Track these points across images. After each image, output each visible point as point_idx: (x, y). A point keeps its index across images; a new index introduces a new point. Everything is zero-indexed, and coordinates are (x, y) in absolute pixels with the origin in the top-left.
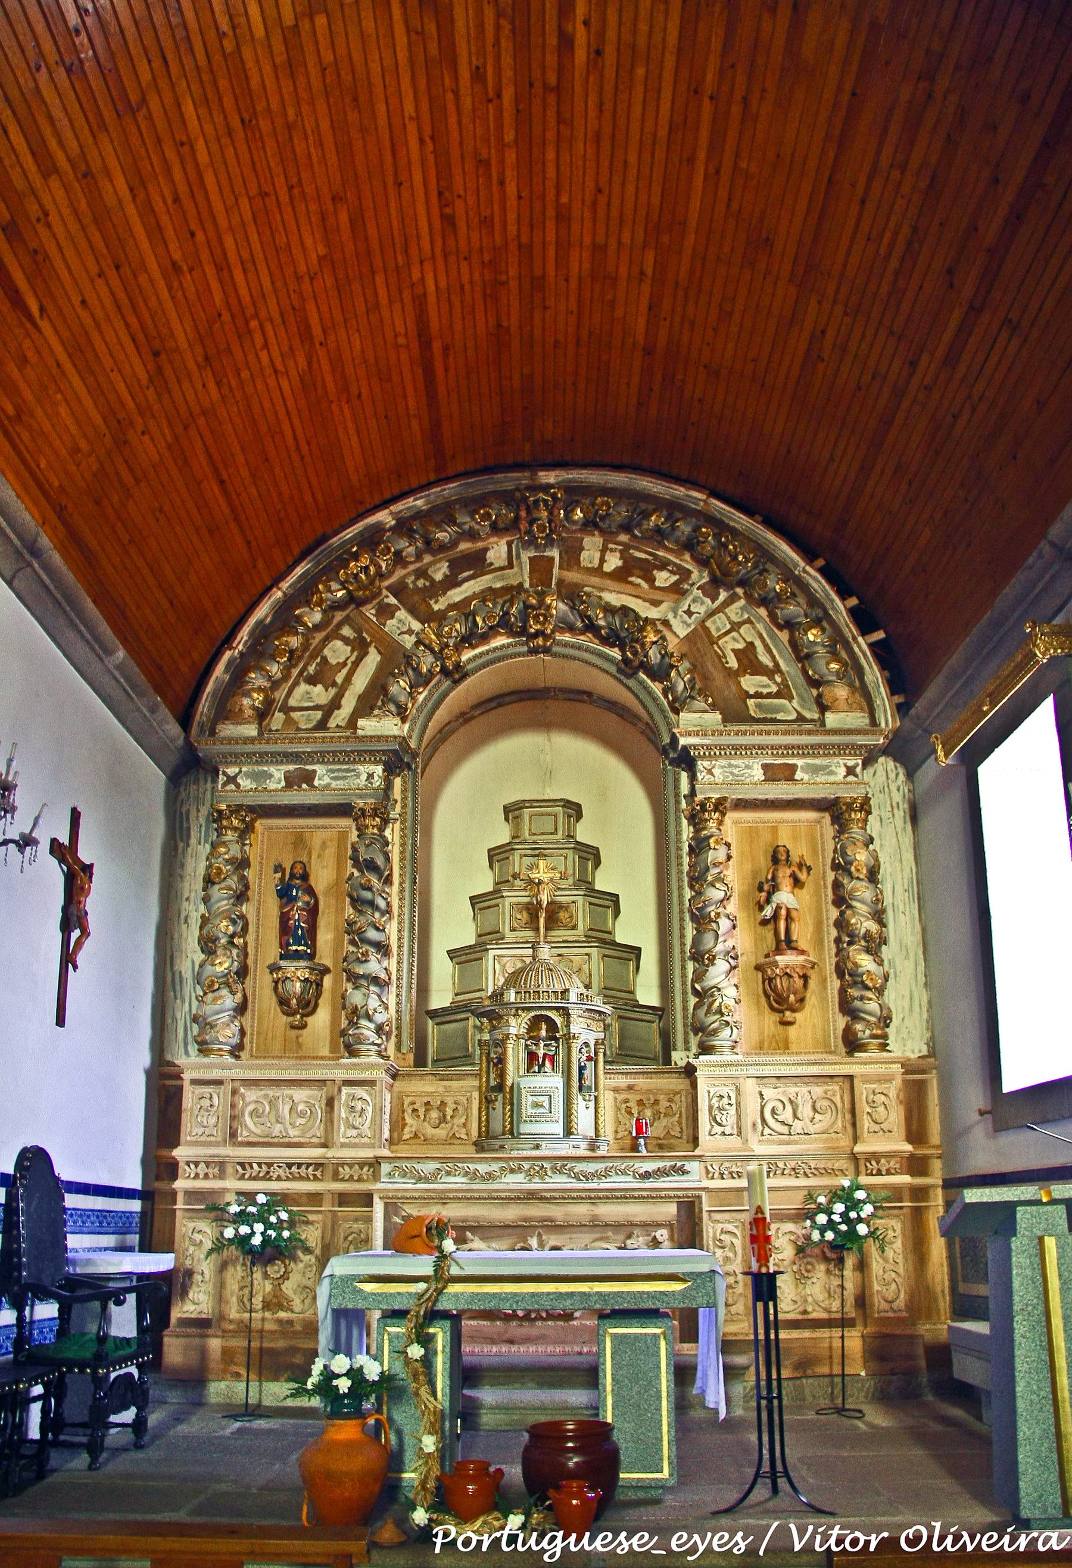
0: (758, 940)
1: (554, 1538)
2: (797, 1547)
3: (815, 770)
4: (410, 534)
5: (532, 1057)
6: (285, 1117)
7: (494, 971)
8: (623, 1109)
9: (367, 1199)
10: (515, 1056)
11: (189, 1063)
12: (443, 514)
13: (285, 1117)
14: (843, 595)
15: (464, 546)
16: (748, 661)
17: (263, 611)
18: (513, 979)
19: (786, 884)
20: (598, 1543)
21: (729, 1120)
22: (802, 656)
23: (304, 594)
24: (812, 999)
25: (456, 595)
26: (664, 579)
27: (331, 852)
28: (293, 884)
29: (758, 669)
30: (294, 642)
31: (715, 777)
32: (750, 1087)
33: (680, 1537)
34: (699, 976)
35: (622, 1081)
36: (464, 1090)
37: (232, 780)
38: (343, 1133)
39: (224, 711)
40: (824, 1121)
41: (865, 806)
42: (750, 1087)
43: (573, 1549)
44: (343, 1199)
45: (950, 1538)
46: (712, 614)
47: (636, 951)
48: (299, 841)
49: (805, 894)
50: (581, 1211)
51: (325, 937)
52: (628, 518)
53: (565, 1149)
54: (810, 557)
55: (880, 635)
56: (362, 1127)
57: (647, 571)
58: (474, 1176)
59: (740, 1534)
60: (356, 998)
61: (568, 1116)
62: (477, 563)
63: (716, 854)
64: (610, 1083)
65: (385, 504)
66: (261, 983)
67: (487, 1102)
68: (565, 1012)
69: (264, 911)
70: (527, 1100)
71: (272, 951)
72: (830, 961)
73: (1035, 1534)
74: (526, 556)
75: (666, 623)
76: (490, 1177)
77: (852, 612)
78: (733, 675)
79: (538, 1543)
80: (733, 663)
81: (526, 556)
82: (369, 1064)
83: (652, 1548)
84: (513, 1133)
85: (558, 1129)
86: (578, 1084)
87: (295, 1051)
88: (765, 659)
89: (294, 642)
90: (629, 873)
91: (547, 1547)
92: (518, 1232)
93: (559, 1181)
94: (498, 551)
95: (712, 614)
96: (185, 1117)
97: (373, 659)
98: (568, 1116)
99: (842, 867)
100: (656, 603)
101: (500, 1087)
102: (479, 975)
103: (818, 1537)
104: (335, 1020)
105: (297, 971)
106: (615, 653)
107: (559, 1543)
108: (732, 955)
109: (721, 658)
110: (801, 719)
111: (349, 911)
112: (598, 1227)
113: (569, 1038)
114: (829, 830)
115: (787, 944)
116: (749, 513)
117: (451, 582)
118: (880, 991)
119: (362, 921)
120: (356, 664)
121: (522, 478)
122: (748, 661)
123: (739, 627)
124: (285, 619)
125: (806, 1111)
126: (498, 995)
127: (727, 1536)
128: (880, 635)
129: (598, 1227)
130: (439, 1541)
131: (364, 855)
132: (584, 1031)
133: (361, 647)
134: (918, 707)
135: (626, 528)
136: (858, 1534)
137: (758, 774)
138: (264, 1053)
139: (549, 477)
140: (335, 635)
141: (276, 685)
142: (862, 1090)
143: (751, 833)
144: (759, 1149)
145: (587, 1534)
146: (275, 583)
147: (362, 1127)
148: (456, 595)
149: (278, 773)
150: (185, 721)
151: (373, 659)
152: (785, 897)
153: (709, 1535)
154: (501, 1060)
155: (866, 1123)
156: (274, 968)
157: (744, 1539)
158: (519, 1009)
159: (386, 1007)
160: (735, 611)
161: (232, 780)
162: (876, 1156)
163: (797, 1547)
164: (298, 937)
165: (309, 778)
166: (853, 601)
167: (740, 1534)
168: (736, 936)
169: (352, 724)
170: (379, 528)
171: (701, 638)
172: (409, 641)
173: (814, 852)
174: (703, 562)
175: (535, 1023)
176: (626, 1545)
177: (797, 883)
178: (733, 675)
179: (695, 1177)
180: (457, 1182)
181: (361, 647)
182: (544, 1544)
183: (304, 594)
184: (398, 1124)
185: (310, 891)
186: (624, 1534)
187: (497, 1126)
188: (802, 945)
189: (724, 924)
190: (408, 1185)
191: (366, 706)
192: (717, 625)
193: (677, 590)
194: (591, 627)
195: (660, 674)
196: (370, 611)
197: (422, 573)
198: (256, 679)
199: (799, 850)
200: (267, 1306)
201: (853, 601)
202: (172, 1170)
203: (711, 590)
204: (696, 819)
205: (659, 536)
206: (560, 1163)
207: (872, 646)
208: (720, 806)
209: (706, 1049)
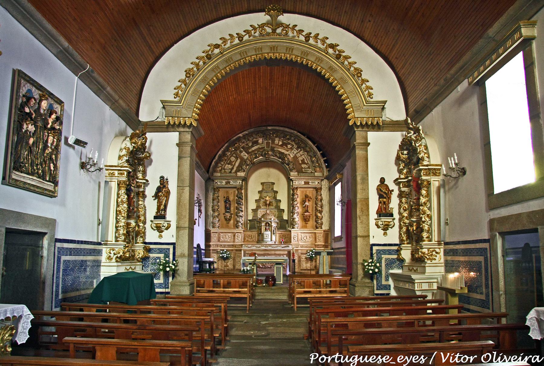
0: (303, 210)
1: (354, 358)
2: (444, 361)
3: (312, 182)
4: (245, 138)
5: (266, 229)
6: (227, 238)
7: (260, 213)
8: (280, 237)
9: (241, 250)
10: (263, 228)
11: (212, 230)
12: (250, 135)
13: (227, 238)
14: (319, 151)
15: (255, 140)
16: (303, 161)
17: (220, 152)
18: (263, 216)
19: (307, 201)
20: (370, 360)
21: (296, 239)
22: (313, 162)
23: (227, 149)
24: (311, 220)
25: (253, 149)
26: (289, 146)
27: (232, 194)
28: (227, 201)
29: (305, 163)
30: (226, 158)
31: (296, 183)
32: (300, 234)
33: (401, 357)
34: (292, 216)
35: (280, 232)
36: (254, 233)
37: (216, 183)
38: (236, 240)
39: (215, 171)
40: (311, 239)
41: (321, 189)
42: (300, 234)
43: (361, 362)
44: (237, 250)
45: (500, 358)
46: (297, 153)
47: (283, 210)
48: (227, 192)
49: (311, 202)
50: (273, 252)
51: (232, 208)
52: (283, 136)
53: (270, 243)
54: (314, 144)
55: (325, 158)
56: (239, 240)
57: (286, 145)
58: (257, 247)
59: (423, 356)
60: (238, 219)
61: (271, 238)
62: (256, 143)
63: (296, 196)
64: (278, 233)
65: (241, 133)
66: (222, 217)
67: (259, 235)
68: (271, 222)
69: (222, 204)
70: (265, 235)
71: (223, 211)
72: (314, 214)
73: (531, 356)
74: (265, 142)
75: (289, 155)
76: (259, 247)
77: (321, 154)
78: (300, 164)
79: (348, 360)
80: (300, 162)
81: (265, 142)
82: (241, 229)
83: (391, 361)
84: (263, 240)
85: (270, 240)
86: (273, 233)
87: (227, 227)
88: (306, 162)
89: (226, 158)
90: (283, 196)
91: (352, 361)
92: (264, 255)
93: (270, 248)
94: (260, 141)
95: (297, 153)
96: (212, 238)
97: (239, 160)
98: (271, 238)
99: (317, 199)
100: (288, 151)
101: (261, 233)
102: (257, 214)
103: (451, 357)
104: (234, 222)
105: (228, 215)
106: (280, 160)
107: (356, 360)
108: (298, 213)
109: (298, 161)
110: (312, 172)
111: (236, 205)
112: (275, 255)
113: (271, 226)
114: (315, 192)
115: (307, 211)
116: (304, 135)
117: (252, 146)
118: (322, 219)
119: (238, 207)
120: (236, 161)
121: (265, 128)
122: (303, 161)
123: (302, 156)
124: (224, 154)
125: (308, 238)
126: (260, 219)
127: (418, 357)
128: (325, 158)
129: (275, 255)
130: (312, 359)
131: (239, 196)
132: (274, 225)
133: (237, 158)
134: (332, 171)
135: (283, 137)
136: (466, 356)
137: (303, 183)
138: (222, 227)
139: (269, 128)
140: (232, 156)
141: (222, 165)
142: (317, 235)
143: (302, 192)
144: (300, 243)
145: (367, 356)
146: (222, 147)
147: (239, 240)
148: (253, 149)
149: (224, 182)
150: (208, 172)
151: (239, 160)
152: (307, 203)
153: (411, 357)
154: (261, 229)
155: (318, 240)
156: (224, 214)
157: (424, 358)
158: (263, 221)
159: (242, 220)
160: (301, 153)
161: (216, 183)
162: (319, 245)
163: (444, 361)
164: (227, 209)
165: (229, 182)
166: (321, 152)
167: (423, 356)
168: (298, 209)
169: (236, 172)
170: (240, 137)
171: (295, 157)
172: (245, 158)
173: (312, 195)
174: (296, 144)
175: (266, 223)
176: (381, 360)
177: (309, 201)
178: (300, 164)
179: (290, 247)
180: (254, 248)
181: (237, 158)
182: (351, 360)
183: (227, 149)
184: (244, 239)
185: (230, 201)
186: (380, 356)
187: (260, 239)
188: (310, 211)
189: (297, 208)
190: (247, 248)
191: (238, 170)
192: (298, 155)
193: (291, 149)
194: (276, 156)
195: (288, 165)
196: (238, 152)
197: (247, 145)
198: (220, 165)
199: (310, 195)
200: (225, 266)
201: (321, 152)
202: (210, 246)
203: (297, 149)
204: (293, 190)
205: (288, 139)
206: (270, 245)
207: (324, 160)
208: (297, 188)
209: (293, 228)
